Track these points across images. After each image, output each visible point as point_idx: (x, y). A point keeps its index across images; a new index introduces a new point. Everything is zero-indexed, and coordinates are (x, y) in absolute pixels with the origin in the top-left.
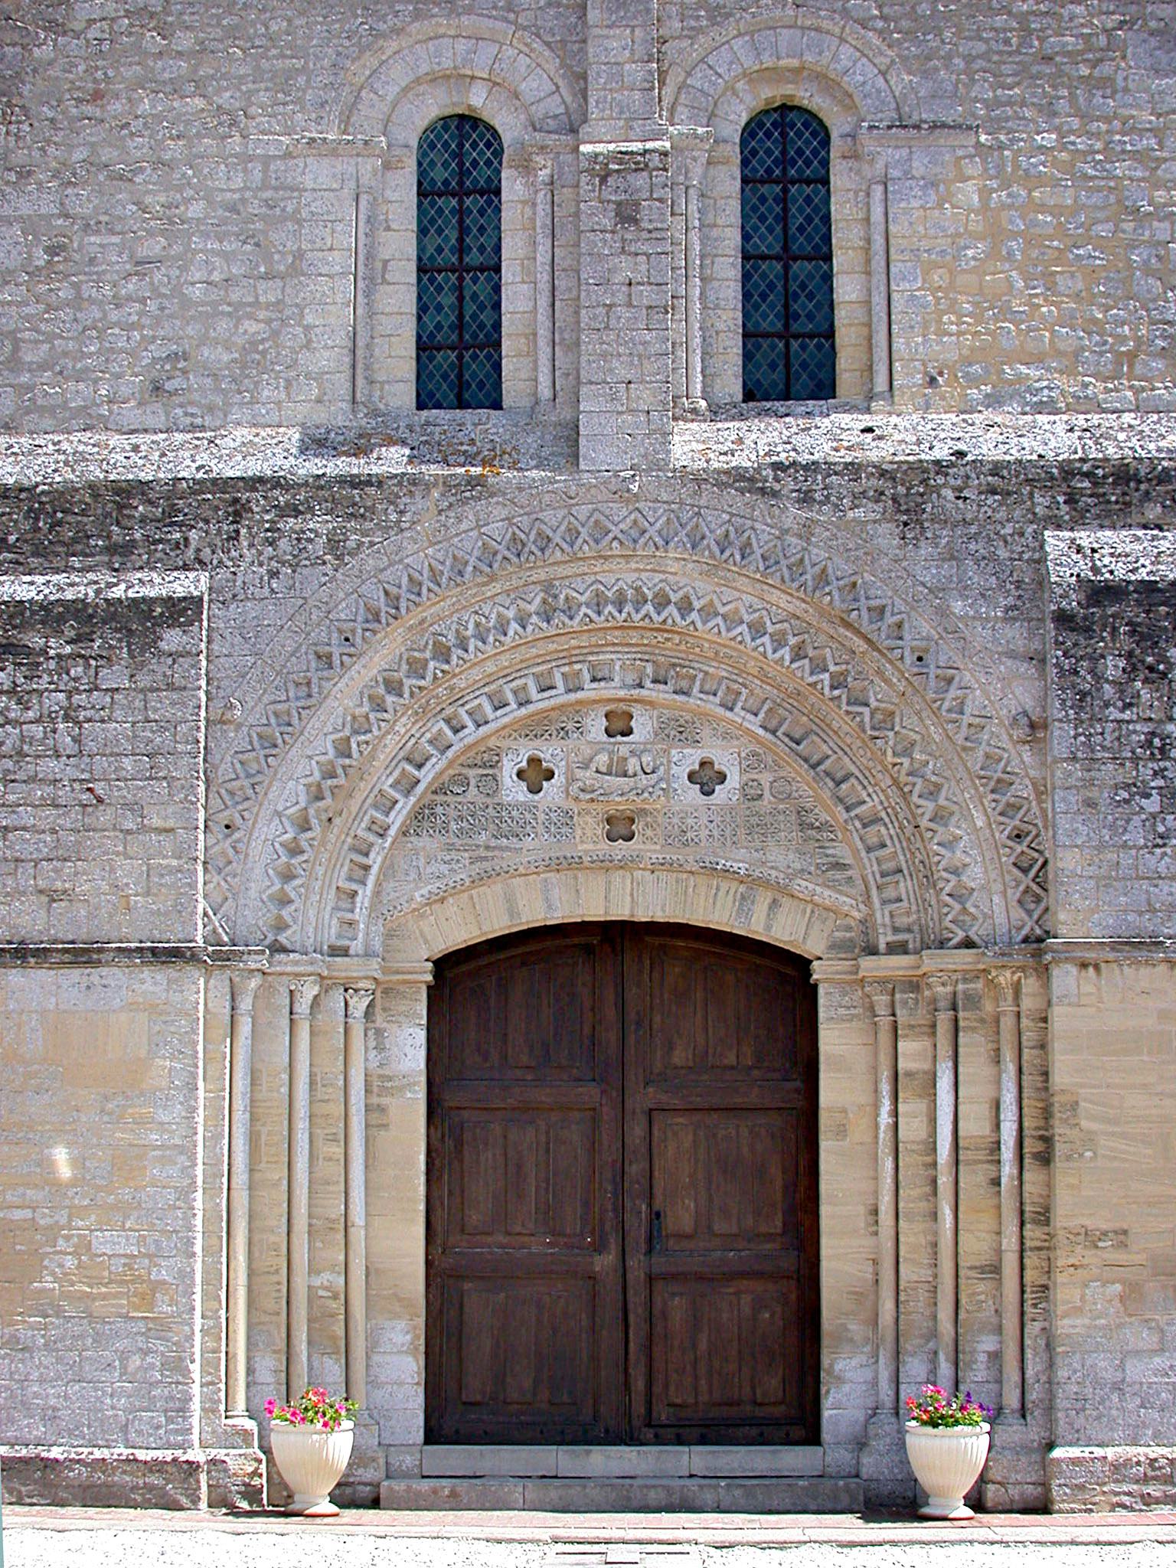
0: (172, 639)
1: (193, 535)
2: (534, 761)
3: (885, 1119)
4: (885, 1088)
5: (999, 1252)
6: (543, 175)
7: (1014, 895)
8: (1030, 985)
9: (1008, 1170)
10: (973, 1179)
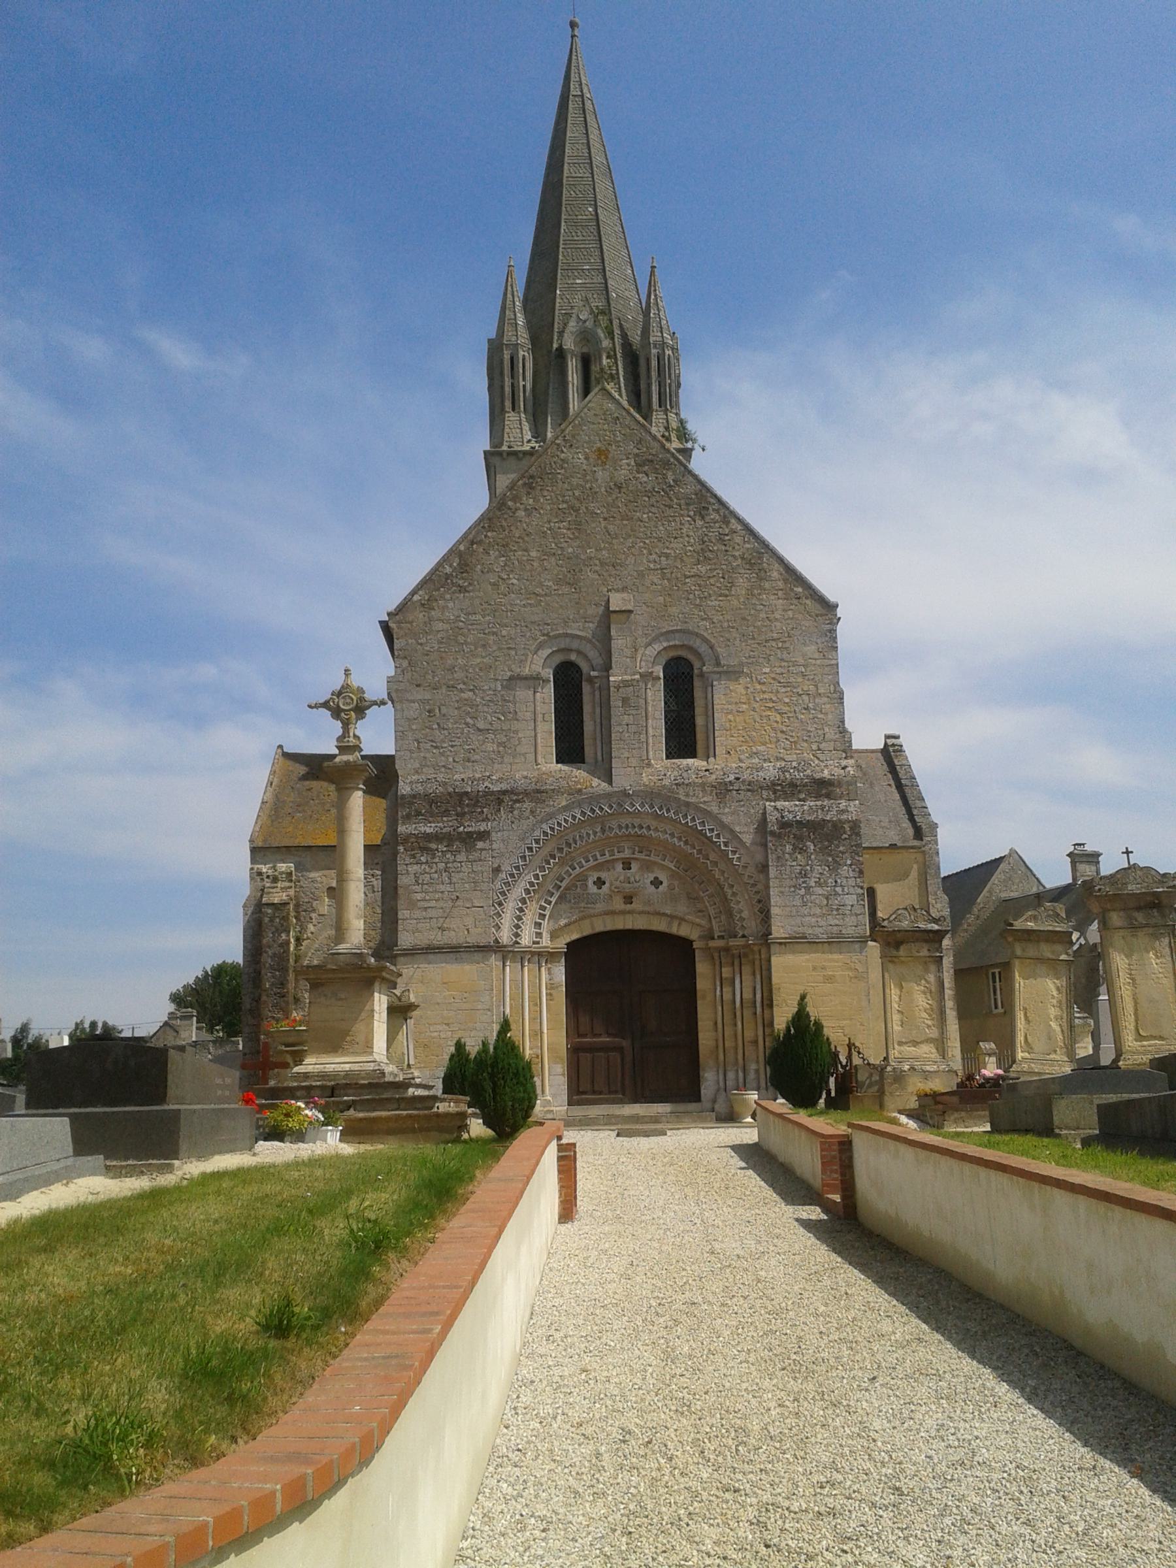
0: (480, 845)
1: (485, 810)
2: (599, 878)
3: (718, 993)
4: (718, 983)
5: (757, 1036)
6: (597, 685)
7: (758, 921)
8: (763, 951)
9: (759, 1010)
10: (748, 1013)
